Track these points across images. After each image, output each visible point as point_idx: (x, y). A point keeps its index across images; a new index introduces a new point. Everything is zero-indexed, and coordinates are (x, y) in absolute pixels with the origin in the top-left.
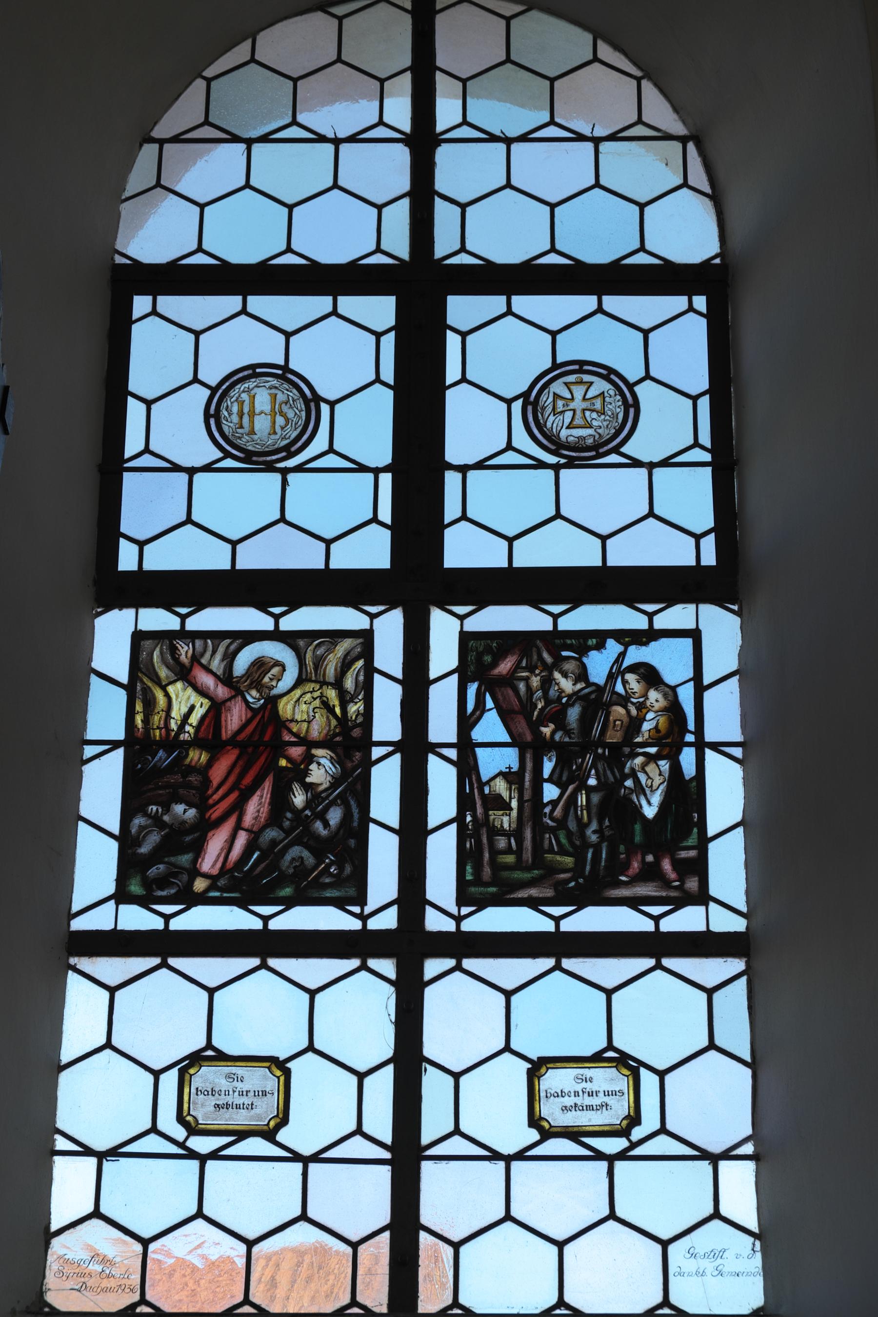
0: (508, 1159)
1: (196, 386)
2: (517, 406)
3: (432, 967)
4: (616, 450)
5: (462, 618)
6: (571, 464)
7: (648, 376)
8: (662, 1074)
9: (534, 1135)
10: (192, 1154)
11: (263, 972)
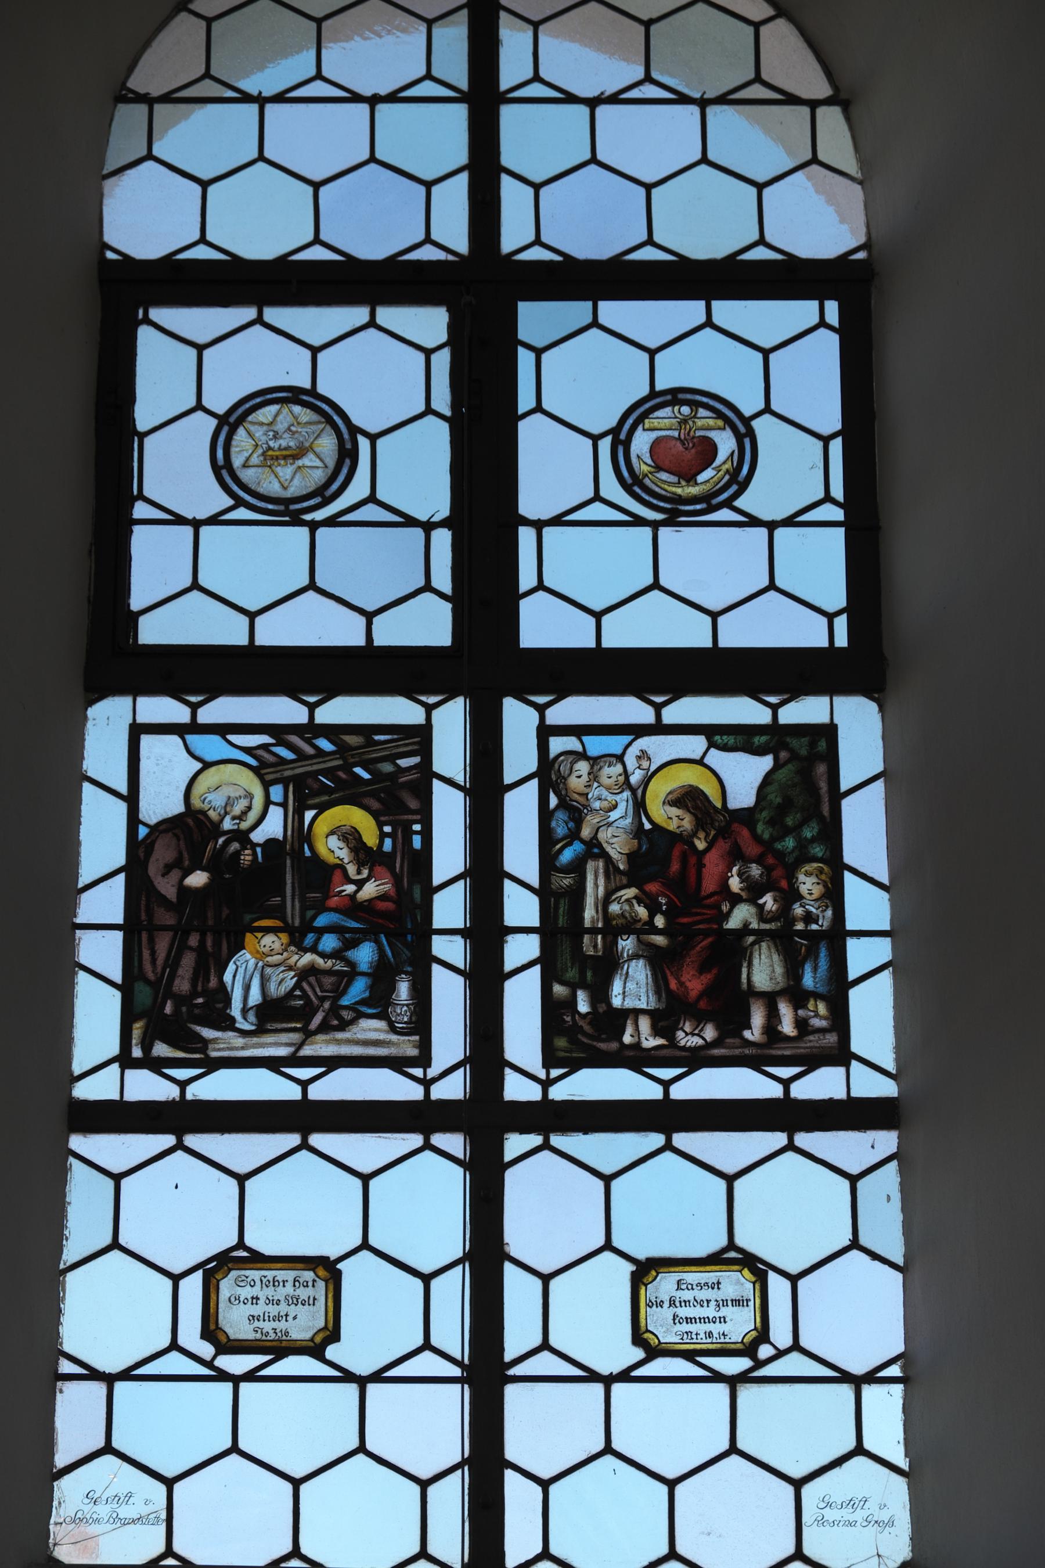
0: (608, 1381)
1: (200, 414)
2: (605, 445)
3: (515, 1144)
4: (728, 504)
5: (541, 709)
6: (672, 520)
7: (768, 409)
8: (794, 1279)
9: (639, 1354)
10: (222, 1376)
11: (546, 1154)
